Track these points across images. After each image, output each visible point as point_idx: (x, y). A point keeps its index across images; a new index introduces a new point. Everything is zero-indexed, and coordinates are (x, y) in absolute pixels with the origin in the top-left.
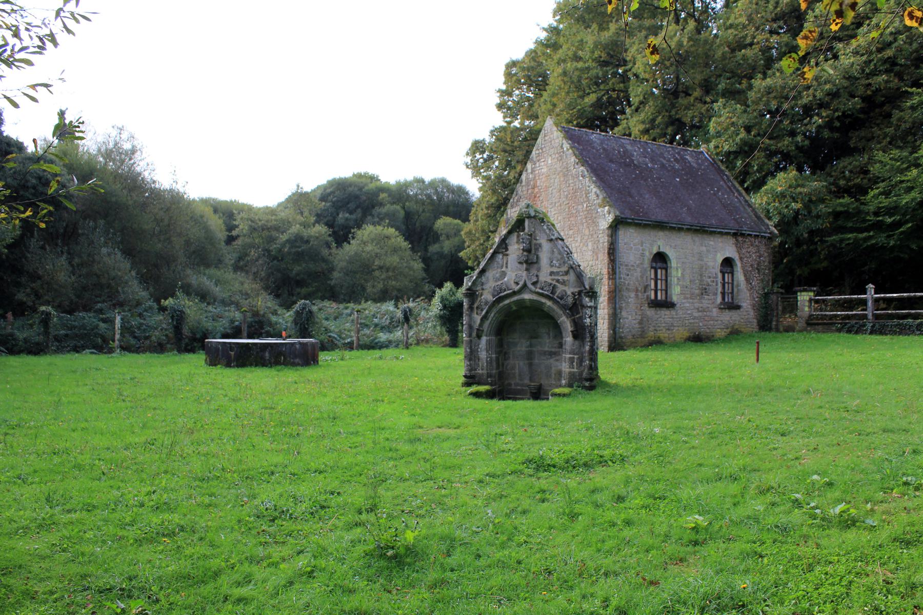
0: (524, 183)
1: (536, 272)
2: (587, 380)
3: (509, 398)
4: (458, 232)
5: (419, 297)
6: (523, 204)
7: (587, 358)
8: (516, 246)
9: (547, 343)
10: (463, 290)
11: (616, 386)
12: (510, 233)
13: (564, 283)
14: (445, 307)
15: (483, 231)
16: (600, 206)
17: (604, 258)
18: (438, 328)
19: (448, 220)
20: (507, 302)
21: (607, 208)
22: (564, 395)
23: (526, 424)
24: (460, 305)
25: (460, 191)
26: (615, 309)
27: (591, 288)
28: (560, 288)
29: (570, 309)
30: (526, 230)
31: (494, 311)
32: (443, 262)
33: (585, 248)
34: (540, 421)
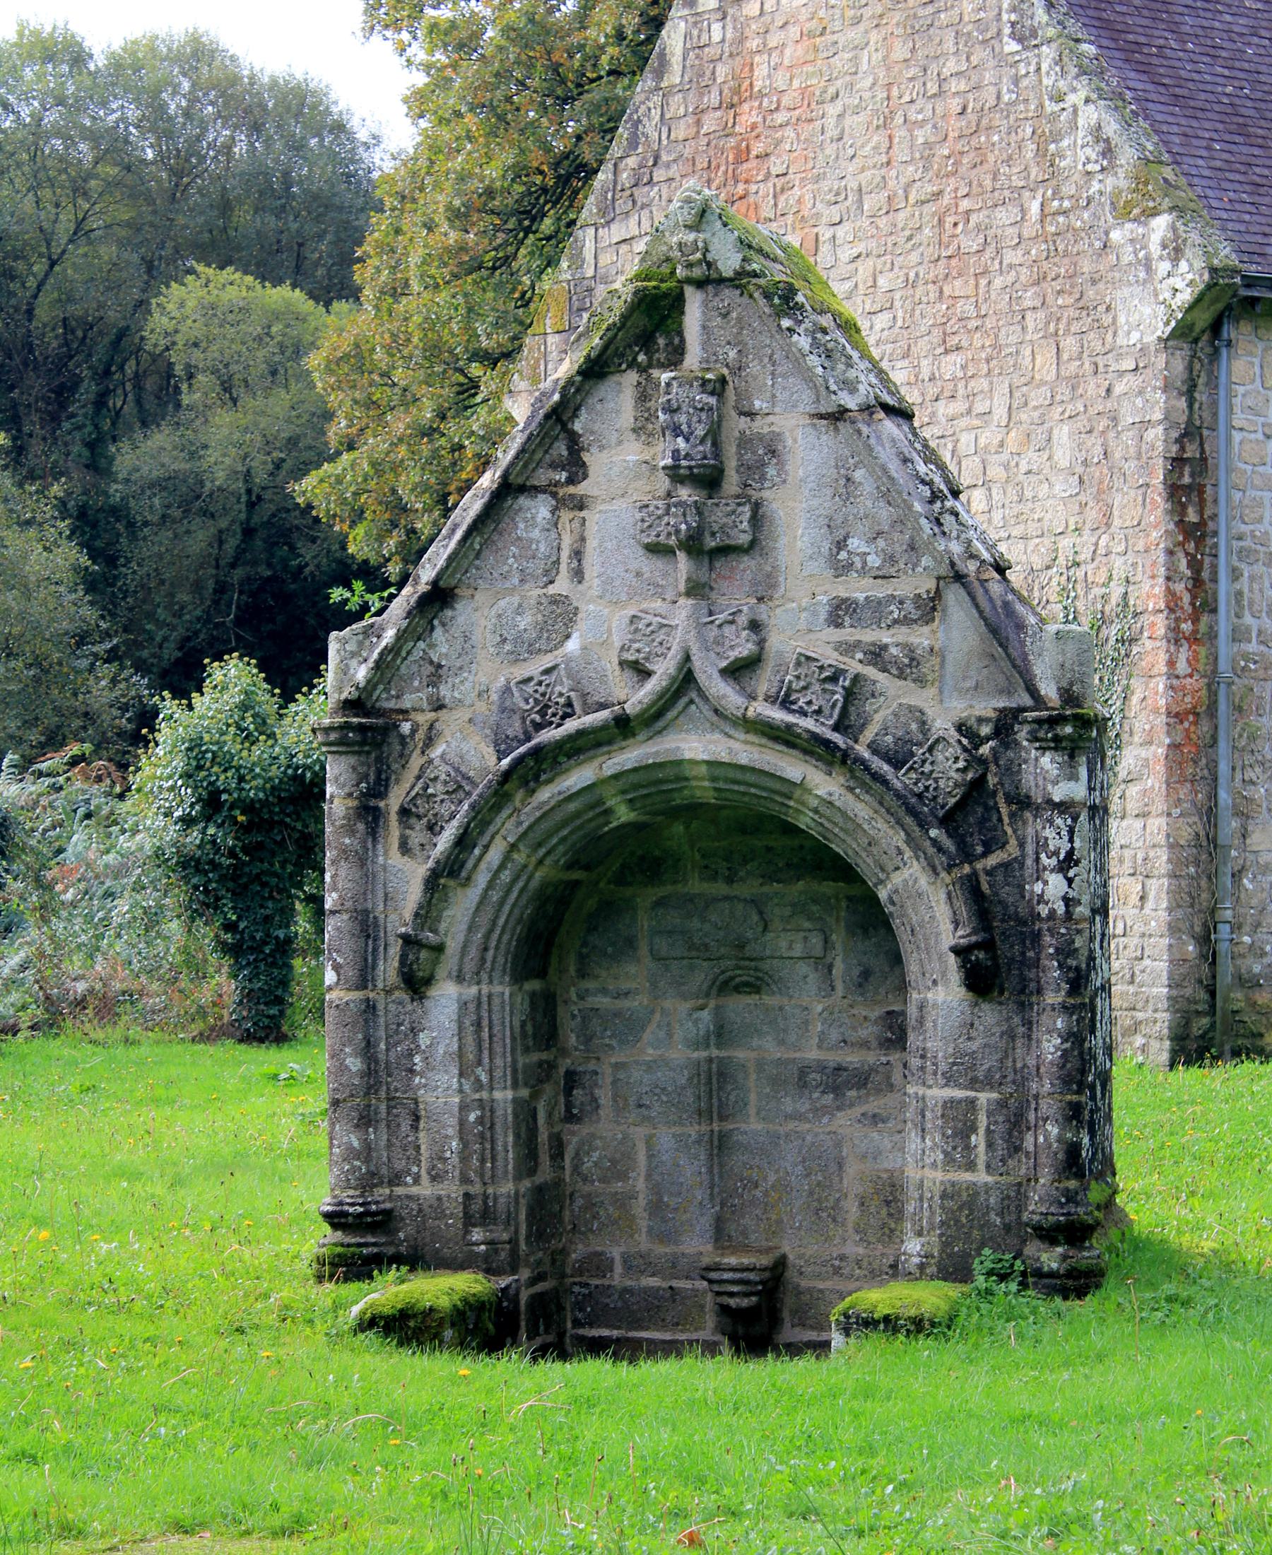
0: (674, 77)
1: (747, 605)
2: (1049, 1235)
3: (596, 1347)
4: (284, 364)
5: (54, 741)
6: (668, 202)
7: (1049, 1106)
8: (632, 452)
9: (811, 1014)
10: (317, 710)
11: (1225, 1267)
12: (595, 370)
13: (909, 667)
14: (212, 803)
15: (434, 351)
16: (1123, 212)
17: (1143, 518)
18: (174, 927)
19: (232, 286)
20: (578, 777)
21: (1161, 224)
22: (919, 1326)
23: (697, 1501)
24: (305, 792)
25: (297, 114)
26: (1210, 813)
27: (1069, 697)
28: (890, 700)
29: (948, 820)
30: (693, 358)
31: (507, 828)
32: (199, 538)
33: (1030, 459)
34: (780, 1485)
